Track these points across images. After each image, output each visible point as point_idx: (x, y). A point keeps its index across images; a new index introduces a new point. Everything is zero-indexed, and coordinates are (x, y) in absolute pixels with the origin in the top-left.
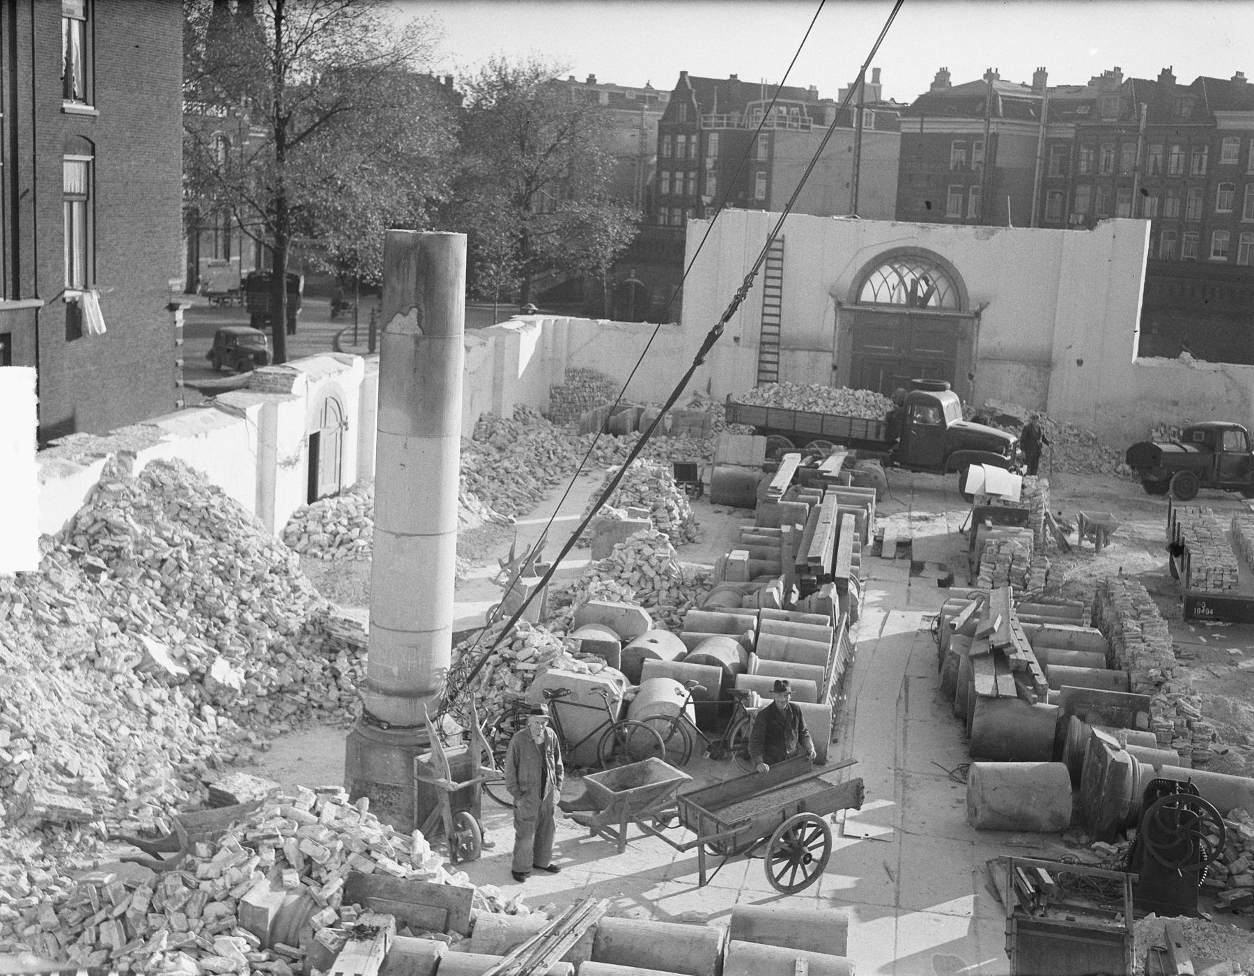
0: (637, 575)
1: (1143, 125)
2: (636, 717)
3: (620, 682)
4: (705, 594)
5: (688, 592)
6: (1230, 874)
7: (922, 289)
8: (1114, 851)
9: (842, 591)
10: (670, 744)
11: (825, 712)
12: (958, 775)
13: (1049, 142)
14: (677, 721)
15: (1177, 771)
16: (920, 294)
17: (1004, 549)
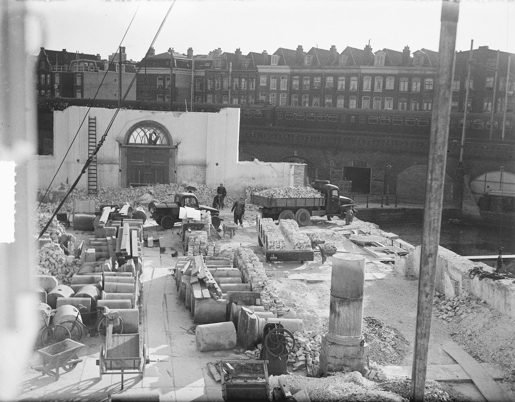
0: (47, 263)
1: (231, 70)
2: (57, 322)
3: (48, 309)
4: (78, 268)
5: (70, 268)
6: (296, 357)
7: (154, 137)
8: (254, 353)
9: (136, 262)
10: (73, 332)
11: (135, 312)
12: (190, 331)
13: (196, 77)
14: (75, 323)
15: (274, 320)
16: (153, 139)
17: (197, 240)
